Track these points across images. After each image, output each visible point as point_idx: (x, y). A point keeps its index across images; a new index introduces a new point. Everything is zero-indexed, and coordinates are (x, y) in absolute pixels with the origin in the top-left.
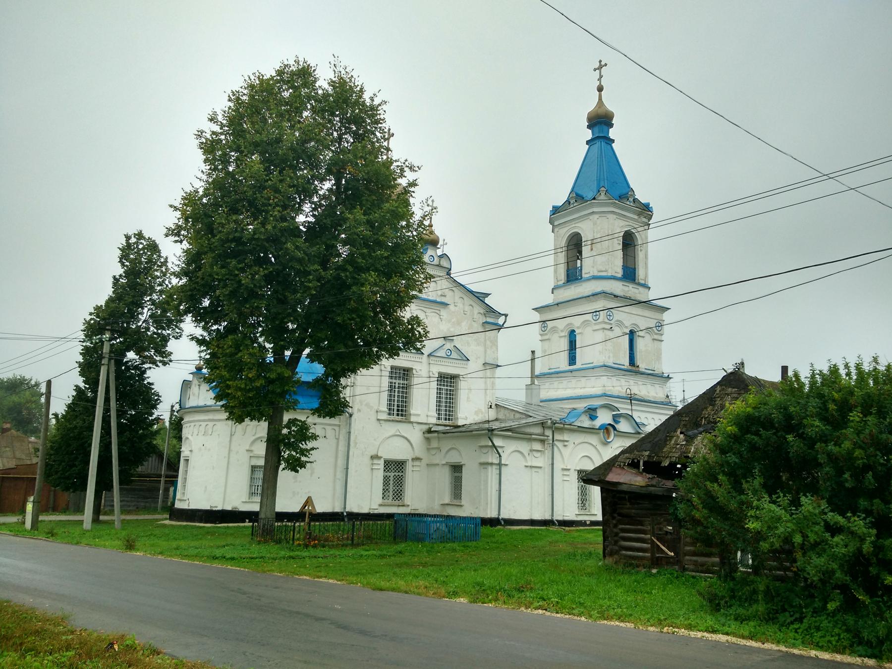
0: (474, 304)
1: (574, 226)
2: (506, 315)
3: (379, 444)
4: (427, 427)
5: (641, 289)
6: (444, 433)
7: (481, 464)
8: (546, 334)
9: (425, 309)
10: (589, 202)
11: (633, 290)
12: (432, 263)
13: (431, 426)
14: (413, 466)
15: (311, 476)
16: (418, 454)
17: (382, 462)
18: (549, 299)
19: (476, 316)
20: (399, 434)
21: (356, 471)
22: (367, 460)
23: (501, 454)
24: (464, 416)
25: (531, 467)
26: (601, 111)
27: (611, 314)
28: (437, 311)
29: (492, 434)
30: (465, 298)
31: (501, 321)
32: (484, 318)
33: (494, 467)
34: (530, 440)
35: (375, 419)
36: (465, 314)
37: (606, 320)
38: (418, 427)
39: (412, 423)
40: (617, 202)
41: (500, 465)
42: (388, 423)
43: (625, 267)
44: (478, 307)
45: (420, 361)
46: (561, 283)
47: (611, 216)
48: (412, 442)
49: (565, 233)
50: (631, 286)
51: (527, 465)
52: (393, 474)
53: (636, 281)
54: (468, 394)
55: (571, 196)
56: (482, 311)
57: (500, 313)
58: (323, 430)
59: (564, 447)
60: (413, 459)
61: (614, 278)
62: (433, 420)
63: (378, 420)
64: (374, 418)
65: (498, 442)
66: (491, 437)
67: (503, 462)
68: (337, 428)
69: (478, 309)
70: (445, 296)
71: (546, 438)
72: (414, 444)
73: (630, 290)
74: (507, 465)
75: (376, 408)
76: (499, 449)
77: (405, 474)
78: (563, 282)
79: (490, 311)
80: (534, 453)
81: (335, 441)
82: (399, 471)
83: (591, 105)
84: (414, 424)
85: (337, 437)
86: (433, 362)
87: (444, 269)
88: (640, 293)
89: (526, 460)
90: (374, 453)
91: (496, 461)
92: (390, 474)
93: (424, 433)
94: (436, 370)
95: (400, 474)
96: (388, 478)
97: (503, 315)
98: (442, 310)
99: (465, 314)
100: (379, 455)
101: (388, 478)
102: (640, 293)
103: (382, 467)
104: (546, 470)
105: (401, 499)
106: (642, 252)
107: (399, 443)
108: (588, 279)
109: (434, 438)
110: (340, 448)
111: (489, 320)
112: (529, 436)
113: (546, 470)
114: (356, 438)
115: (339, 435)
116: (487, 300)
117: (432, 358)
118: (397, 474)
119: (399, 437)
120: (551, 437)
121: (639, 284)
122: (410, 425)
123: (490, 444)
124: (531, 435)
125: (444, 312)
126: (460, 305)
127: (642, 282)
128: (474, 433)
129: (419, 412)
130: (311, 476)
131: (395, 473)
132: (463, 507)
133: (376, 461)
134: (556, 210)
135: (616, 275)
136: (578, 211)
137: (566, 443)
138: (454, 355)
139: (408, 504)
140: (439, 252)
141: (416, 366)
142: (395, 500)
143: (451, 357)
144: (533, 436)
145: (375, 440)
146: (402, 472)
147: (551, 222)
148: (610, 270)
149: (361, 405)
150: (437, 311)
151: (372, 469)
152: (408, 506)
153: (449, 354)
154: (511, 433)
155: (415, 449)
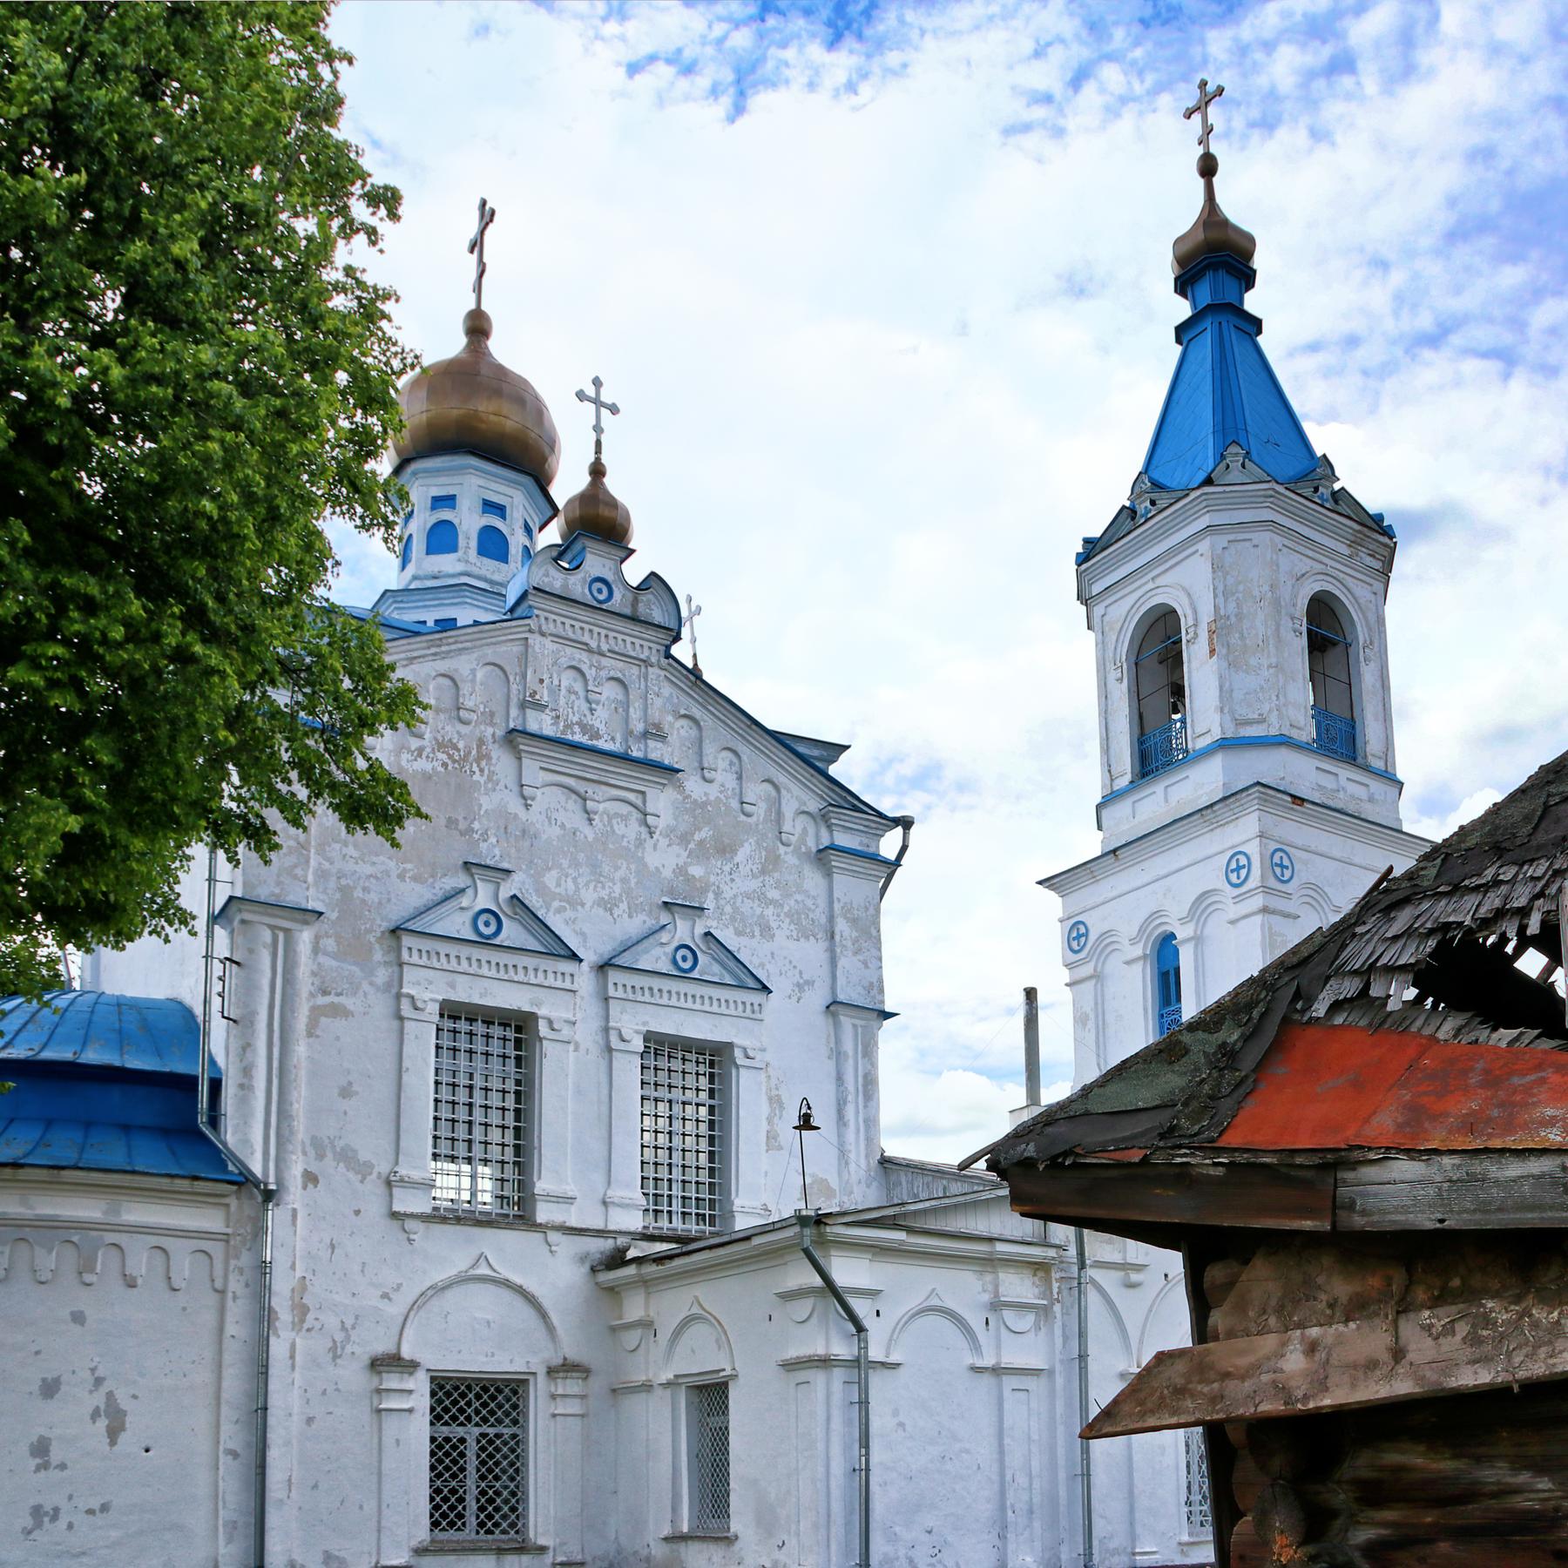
0: (781, 779)
1: (1152, 585)
2: (906, 823)
3: (404, 1310)
4: (607, 1245)
5: (1377, 786)
6: (655, 1260)
7: (790, 1366)
8: (1084, 962)
9: (581, 787)
10: (1193, 495)
11: (1353, 789)
12: (604, 606)
13: (621, 1241)
14: (553, 1397)
15: (113, 1443)
16: (571, 1348)
17: (420, 1385)
18: (1090, 845)
19: (795, 826)
20: (486, 1271)
21: (310, 1420)
22: (353, 1375)
23: (868, 1321)
24: (758, 1204)
25: (997, 1371)
26: (1215, 235)
27: (1286, 862)
28: (631, 797)
29: (824, 1243)
30: (744, 750)
31: (889, 845)
32: (824, 832)
33: (839, 1374)
34: (990, 1263)
35: (384, 1210)
36: (748, 815)
37: (1273, 883)
38: (568, 1247)
39: (542, 1228)
40: (1281, 489)
41: (860, 1365)
42: (438, 1229)
43: (1321, 712)
44: (797, 790)
45: (567, 985)
46: (1123, 782)
47: (1264, 537)
48: (547, 1304)
49: (1126, 611)
50: (1345, 773)
51: (980, 1363)
52: (477, 1431)
53: (1360, 760)
54: (770, 1120)
55: (1136, 490)
56: (814, 805)
57: (880, 815)
58: (159, 1255)
59: (1124, 1291)
60: (551, 1372)
61: (1283, 741)
62: (634, 1221)
63: (395, 1215)
64: (374, 1208)
65: (847, 1271)
66: (817, 1254)
67: (875, 1353)
68: (216, 1249)
69: (799, 796)
70: (662, 738)
71: (1052, 1253)
72: (555, 1319)
73: (1344, 783)
74: (895, 1366)
75: (383, 1167)
76: (855, 1303)
77: (525, 1429)
78: (1128, 777)
79: (847, 802)
80: (1008, 1315)
81: (211, 1299)
82: (499, 1421)
83: (1185, 215)
84: (553, 1236)
85: (218, 1285)
86: (620, 993)
87: (651, 634)
88: (1371, 800)
89: (976, 1346)
90: (383, 1346)
91: (842, 1349)
92: (460, 1432)
93: (593, 1270)
94: (633, 1023)
95: (507, 1432)
96: (454, 1447)
97: (896, 822)
98: (651, 793)
99: (748, 815)
100: (406, 1353)
101: (454, 1447)
102: (1371, 800)
103: (422, 1401)
104: (1060, 1380)
105: (513, 1525)
106: (1372, 665)
107: (484, 1304)
108: (1207, 752)
109: (631, 1284)
110: (231, 1329)
111: (843, 839)
112: (983, 1248)
113: (1060, 1380)
114: (304, 1289)
115: (226, 1277)
116: (833, 770)
117: (614, 976)
118: (491, 1431)
119: (491, 1287)
120: (1072, 1251)
121: (1367, 769)
122: (536, 1237)
123: (817, 1281)
124: (991, 1240)
125: (662, 801)
126: (724, 777)
127: (1378, 764)
128: (756, 1241)
129: (570, 1189)
130: (113, 1443)
131: (485, 1429)
132: (737, 1546)
133: (392, 1381)
134: (1091, 549)
135: (1295, 734)
136: (1165, 532)
137: (1135, 1277)
138: (707, 966)
139: (541, 1541)
140: (634, 572)
141: (548, 1008)
142: (489, 1532)
143: (695, 974)
144: (1001, 1247)
145: (385, 1296)
146: (515, 1422)
147: (1084, 598)
148: (1273, 719)
149: (321, 1157)
150: (631, 797)
151: (379, 1411)
152: (542, 1549)
153: (687, 966)
154: (900, 1236)
155: (560, 1331)
